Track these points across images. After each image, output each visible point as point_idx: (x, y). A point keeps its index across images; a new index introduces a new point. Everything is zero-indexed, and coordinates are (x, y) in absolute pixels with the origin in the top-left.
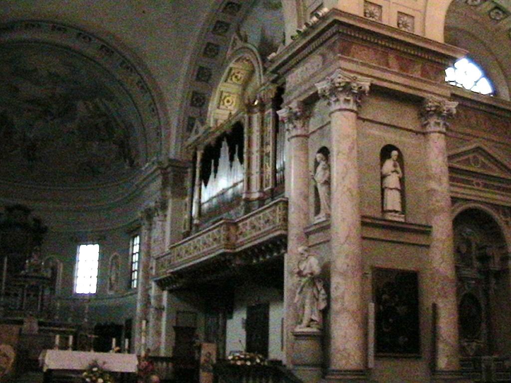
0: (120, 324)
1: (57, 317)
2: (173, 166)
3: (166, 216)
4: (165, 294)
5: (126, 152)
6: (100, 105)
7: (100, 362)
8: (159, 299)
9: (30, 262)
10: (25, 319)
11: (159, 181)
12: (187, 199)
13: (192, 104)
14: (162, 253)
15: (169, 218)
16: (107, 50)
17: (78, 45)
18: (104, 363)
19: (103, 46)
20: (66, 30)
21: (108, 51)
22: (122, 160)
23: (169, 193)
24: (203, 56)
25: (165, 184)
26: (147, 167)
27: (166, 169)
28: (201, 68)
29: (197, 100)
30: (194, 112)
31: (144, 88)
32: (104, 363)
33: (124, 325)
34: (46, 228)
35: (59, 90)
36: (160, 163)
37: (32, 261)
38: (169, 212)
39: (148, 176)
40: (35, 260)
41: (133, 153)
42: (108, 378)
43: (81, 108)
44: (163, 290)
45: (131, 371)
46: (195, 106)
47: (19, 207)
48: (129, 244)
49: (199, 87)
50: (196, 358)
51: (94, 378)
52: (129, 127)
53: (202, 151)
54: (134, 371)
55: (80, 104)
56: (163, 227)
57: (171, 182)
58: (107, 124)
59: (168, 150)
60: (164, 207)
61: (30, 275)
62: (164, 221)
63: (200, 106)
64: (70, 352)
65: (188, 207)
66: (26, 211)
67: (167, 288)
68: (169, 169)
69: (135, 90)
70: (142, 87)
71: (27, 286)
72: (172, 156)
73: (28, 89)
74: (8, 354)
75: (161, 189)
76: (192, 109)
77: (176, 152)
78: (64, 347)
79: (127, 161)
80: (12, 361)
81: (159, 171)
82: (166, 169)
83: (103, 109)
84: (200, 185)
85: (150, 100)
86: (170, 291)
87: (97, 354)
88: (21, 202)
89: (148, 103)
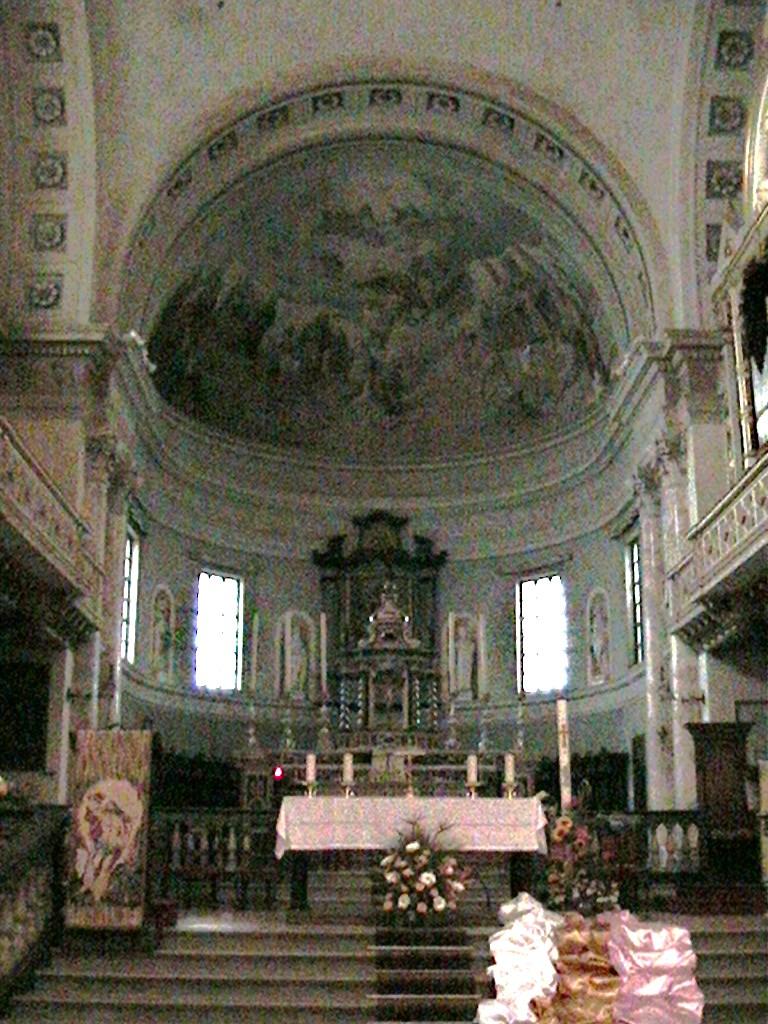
0: (620, 751)
1: (451, 741)
2: (682, 347)
3: (684, 472)
4: (703, 659)
5: (592, 358)
6: (518, 259)
7: (429, 826)
8: (691, 673)
9: (375, 618)
10: (376, 751)
11: (658, 395)
12: (730, 421)
13: (711, 194)
14: (684, 558)
15: (691, 476)
16: (501, 119)
17: (440, 124)
18: (443, 828)
19: (489, 112)
20: (399, 95)
21: (500, 119)
22: (584, 375)
23: (684, 415)
24: (716, 67)
25: (672, 398)
26: (627, 365)
27: (668, 358)
28: (716, 101)
29: (719, 180)
30: (716, 209)
31: (595, 185)
32: (443, 828)
33: (630, 752)
34: (444, 553)
35: (426, 247)
36: (653, 347)
37: (381, 615)
38: (691, 461)
39: (631, 394)
40: (387, 612)
41: (605, 351)
42: (450, 870)
43: (480, 275)
44: (698, 653)
45: (526, 848)
46: (720, 195)
47: (377, 517)
48: (622, 563)
49: (719, 148)
50: (751, 807)
51: (408, 872)
52: (589, 295)
53: (741, 286)
54: (535, 847)
55: (477, 271)
56: (682, 499)
57: (687, 389)
58: (542, 302)
59: (670, 313)
60: (676, 450)
61: (377, 646)
62: (682, 485)
63: (733, 195)
64: (347, 801)
65: (733, 440)
66: (398, 523)
67: (706, 646)
68: (677, 356)
69: (580, 199)
70: (593, 187)
71: (373, 674)
72: (680, 324)
73: (359, 257)
74: (127, 811)
75: (665, 408)
76: (713, 204)
77: (687, 316)
78: (329, 783)
79: (596, 374)
80: (137, 824)
81: (654, 368)
82: (668, 358)
83: (523, 265)
84: (749, 370)
85: (616, 212)
86: (716, 653)
87: (423, 802)
88: (382, 504)
89: (612, 219)
